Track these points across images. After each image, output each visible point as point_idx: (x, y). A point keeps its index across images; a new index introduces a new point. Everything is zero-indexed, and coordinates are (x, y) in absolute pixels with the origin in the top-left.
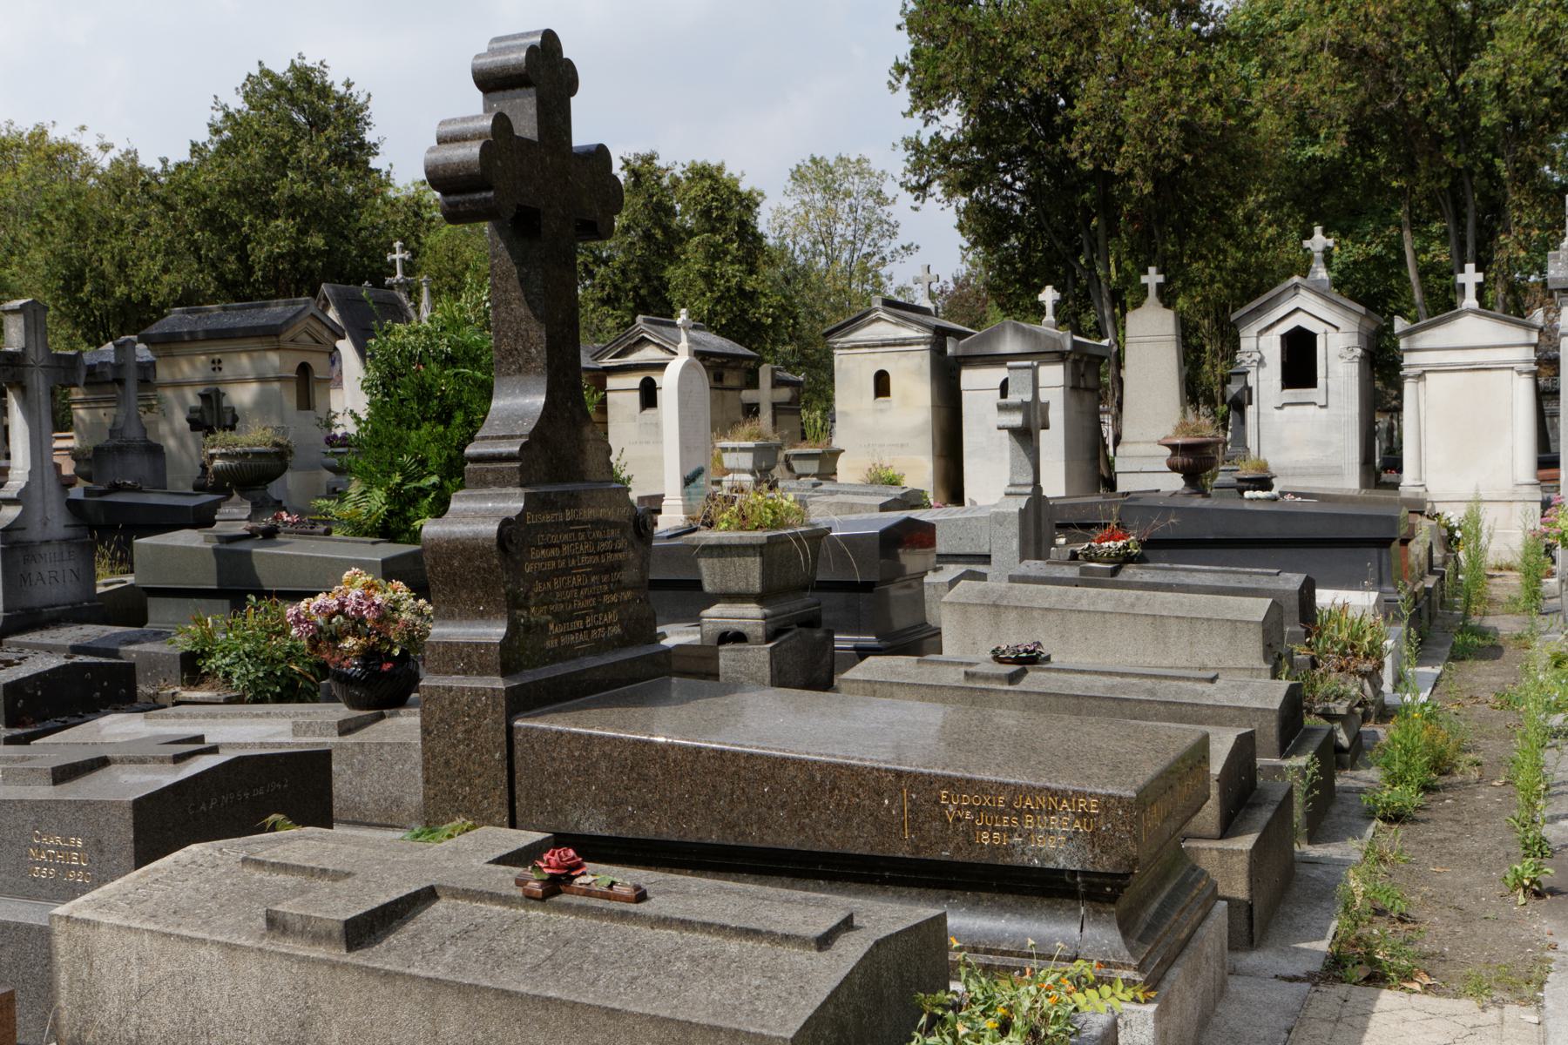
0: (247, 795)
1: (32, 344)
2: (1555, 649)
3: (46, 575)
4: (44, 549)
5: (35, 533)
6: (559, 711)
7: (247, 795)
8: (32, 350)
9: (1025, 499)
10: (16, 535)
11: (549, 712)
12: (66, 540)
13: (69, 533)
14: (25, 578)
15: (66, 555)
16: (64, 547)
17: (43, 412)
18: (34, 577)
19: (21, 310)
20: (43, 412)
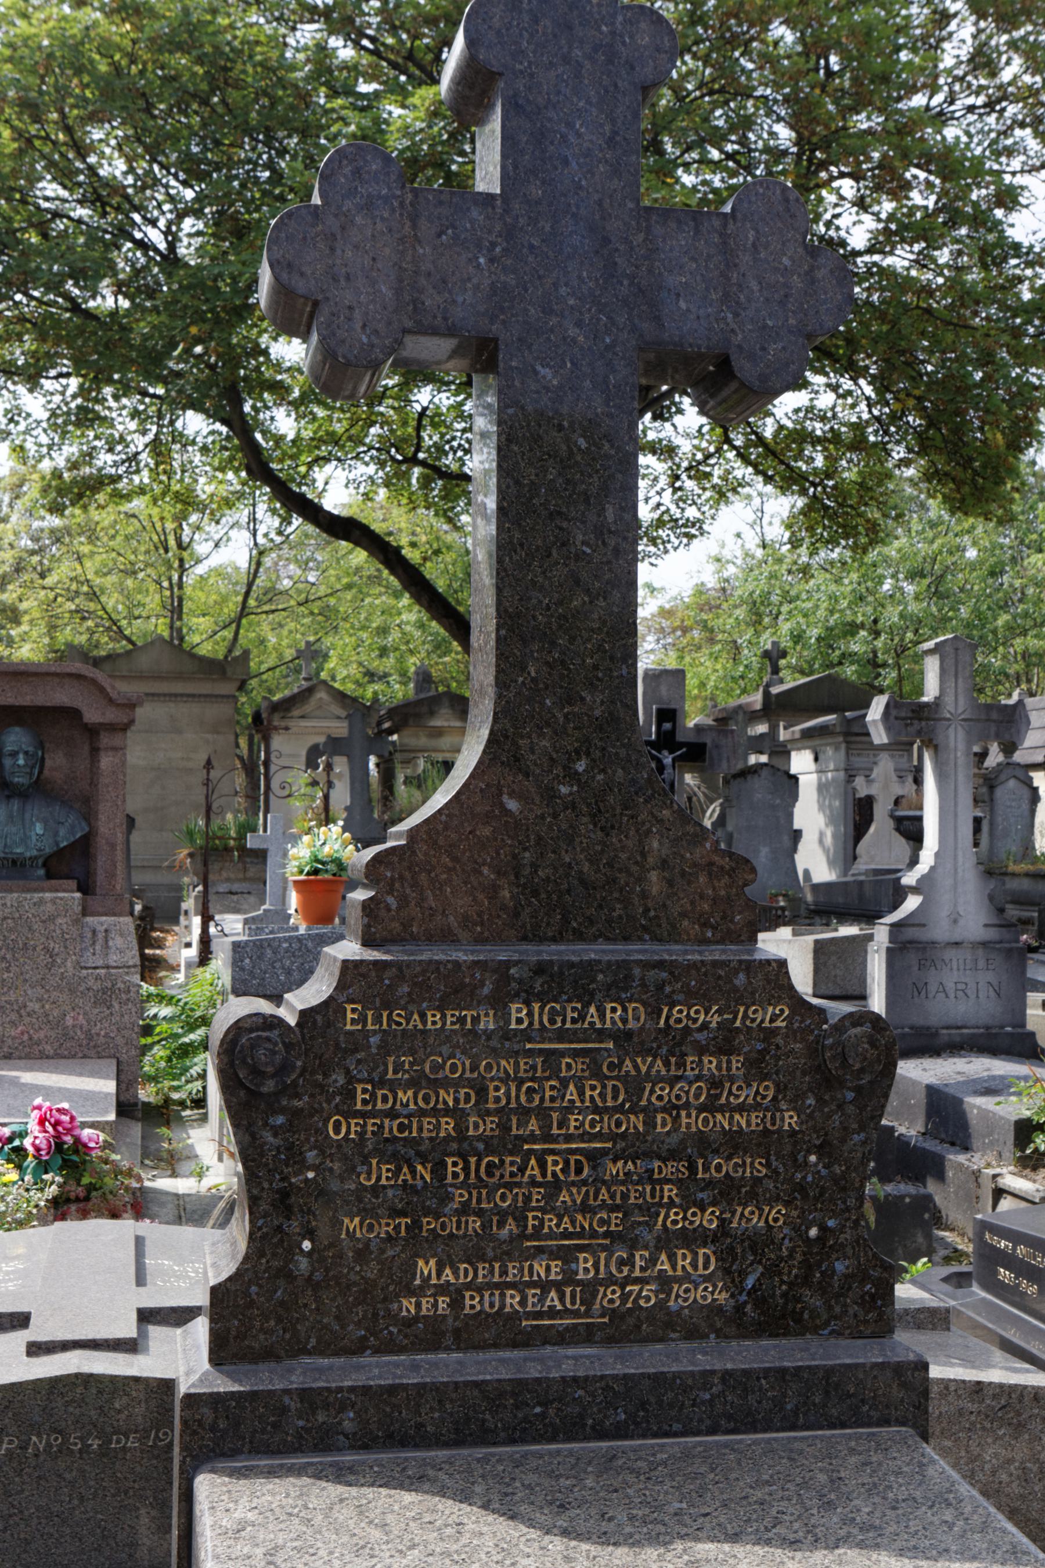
0: (95, 1444)
1: (950, 692)
2: (502, 337)
3: (950, 986)
4: (950, 954)
5: (940, 931)
6: (271, 1473)
7: (95, 1444)
8: (949, 699)
9: (1027, 743)
10: (911, 933)
11: (298, 1471)
12: (984, 944)
13: (992, 934)
14: (920, 988)
15: (981, 963)
16: (980, 952)
17: (961, 778)
18: (933, 988)
19: (936, 649)
20: (961, 778)
